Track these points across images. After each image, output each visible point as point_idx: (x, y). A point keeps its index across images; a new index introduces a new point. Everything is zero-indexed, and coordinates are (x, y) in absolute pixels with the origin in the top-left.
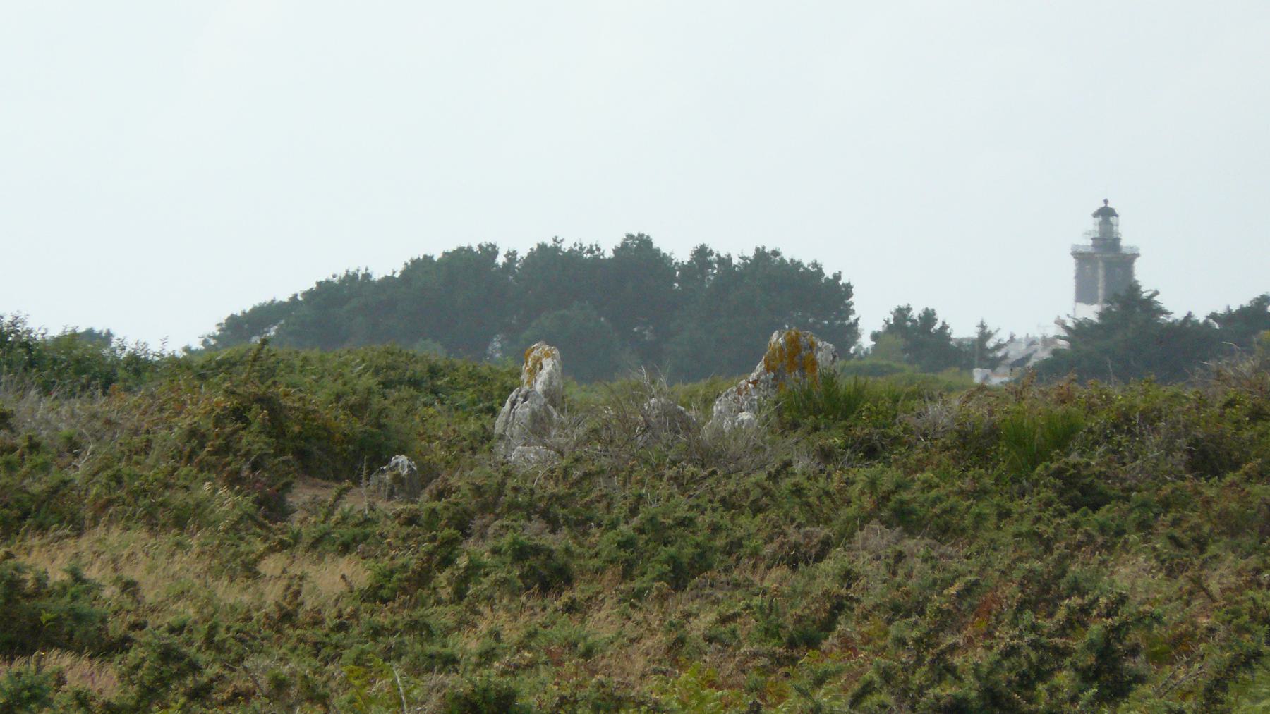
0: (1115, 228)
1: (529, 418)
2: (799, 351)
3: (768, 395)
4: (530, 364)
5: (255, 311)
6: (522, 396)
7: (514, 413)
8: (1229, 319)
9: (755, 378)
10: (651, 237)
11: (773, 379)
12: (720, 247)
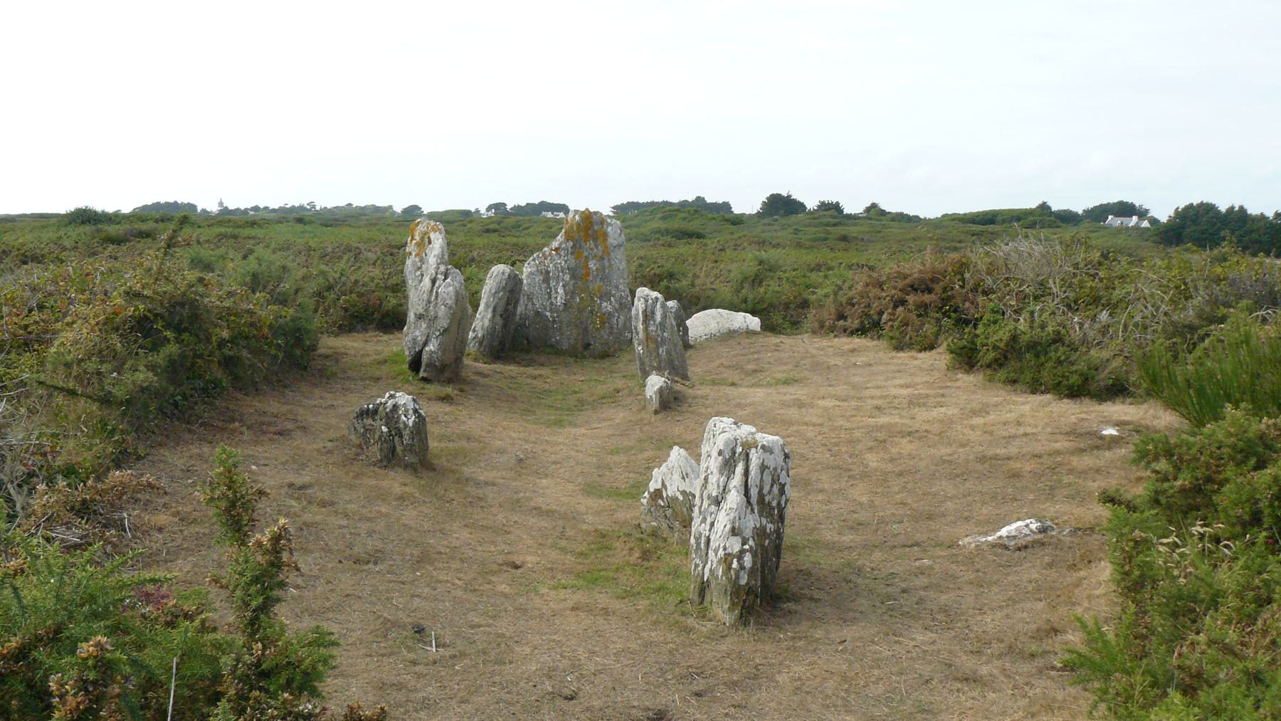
0: (1121, 399)
1: (453, 297)
2: (592, 225)
4: (417, 238)
5: (445, 212)
7: (437, 292)
8: (684, 204)
9: (557, 246)
10: (1245, 207)
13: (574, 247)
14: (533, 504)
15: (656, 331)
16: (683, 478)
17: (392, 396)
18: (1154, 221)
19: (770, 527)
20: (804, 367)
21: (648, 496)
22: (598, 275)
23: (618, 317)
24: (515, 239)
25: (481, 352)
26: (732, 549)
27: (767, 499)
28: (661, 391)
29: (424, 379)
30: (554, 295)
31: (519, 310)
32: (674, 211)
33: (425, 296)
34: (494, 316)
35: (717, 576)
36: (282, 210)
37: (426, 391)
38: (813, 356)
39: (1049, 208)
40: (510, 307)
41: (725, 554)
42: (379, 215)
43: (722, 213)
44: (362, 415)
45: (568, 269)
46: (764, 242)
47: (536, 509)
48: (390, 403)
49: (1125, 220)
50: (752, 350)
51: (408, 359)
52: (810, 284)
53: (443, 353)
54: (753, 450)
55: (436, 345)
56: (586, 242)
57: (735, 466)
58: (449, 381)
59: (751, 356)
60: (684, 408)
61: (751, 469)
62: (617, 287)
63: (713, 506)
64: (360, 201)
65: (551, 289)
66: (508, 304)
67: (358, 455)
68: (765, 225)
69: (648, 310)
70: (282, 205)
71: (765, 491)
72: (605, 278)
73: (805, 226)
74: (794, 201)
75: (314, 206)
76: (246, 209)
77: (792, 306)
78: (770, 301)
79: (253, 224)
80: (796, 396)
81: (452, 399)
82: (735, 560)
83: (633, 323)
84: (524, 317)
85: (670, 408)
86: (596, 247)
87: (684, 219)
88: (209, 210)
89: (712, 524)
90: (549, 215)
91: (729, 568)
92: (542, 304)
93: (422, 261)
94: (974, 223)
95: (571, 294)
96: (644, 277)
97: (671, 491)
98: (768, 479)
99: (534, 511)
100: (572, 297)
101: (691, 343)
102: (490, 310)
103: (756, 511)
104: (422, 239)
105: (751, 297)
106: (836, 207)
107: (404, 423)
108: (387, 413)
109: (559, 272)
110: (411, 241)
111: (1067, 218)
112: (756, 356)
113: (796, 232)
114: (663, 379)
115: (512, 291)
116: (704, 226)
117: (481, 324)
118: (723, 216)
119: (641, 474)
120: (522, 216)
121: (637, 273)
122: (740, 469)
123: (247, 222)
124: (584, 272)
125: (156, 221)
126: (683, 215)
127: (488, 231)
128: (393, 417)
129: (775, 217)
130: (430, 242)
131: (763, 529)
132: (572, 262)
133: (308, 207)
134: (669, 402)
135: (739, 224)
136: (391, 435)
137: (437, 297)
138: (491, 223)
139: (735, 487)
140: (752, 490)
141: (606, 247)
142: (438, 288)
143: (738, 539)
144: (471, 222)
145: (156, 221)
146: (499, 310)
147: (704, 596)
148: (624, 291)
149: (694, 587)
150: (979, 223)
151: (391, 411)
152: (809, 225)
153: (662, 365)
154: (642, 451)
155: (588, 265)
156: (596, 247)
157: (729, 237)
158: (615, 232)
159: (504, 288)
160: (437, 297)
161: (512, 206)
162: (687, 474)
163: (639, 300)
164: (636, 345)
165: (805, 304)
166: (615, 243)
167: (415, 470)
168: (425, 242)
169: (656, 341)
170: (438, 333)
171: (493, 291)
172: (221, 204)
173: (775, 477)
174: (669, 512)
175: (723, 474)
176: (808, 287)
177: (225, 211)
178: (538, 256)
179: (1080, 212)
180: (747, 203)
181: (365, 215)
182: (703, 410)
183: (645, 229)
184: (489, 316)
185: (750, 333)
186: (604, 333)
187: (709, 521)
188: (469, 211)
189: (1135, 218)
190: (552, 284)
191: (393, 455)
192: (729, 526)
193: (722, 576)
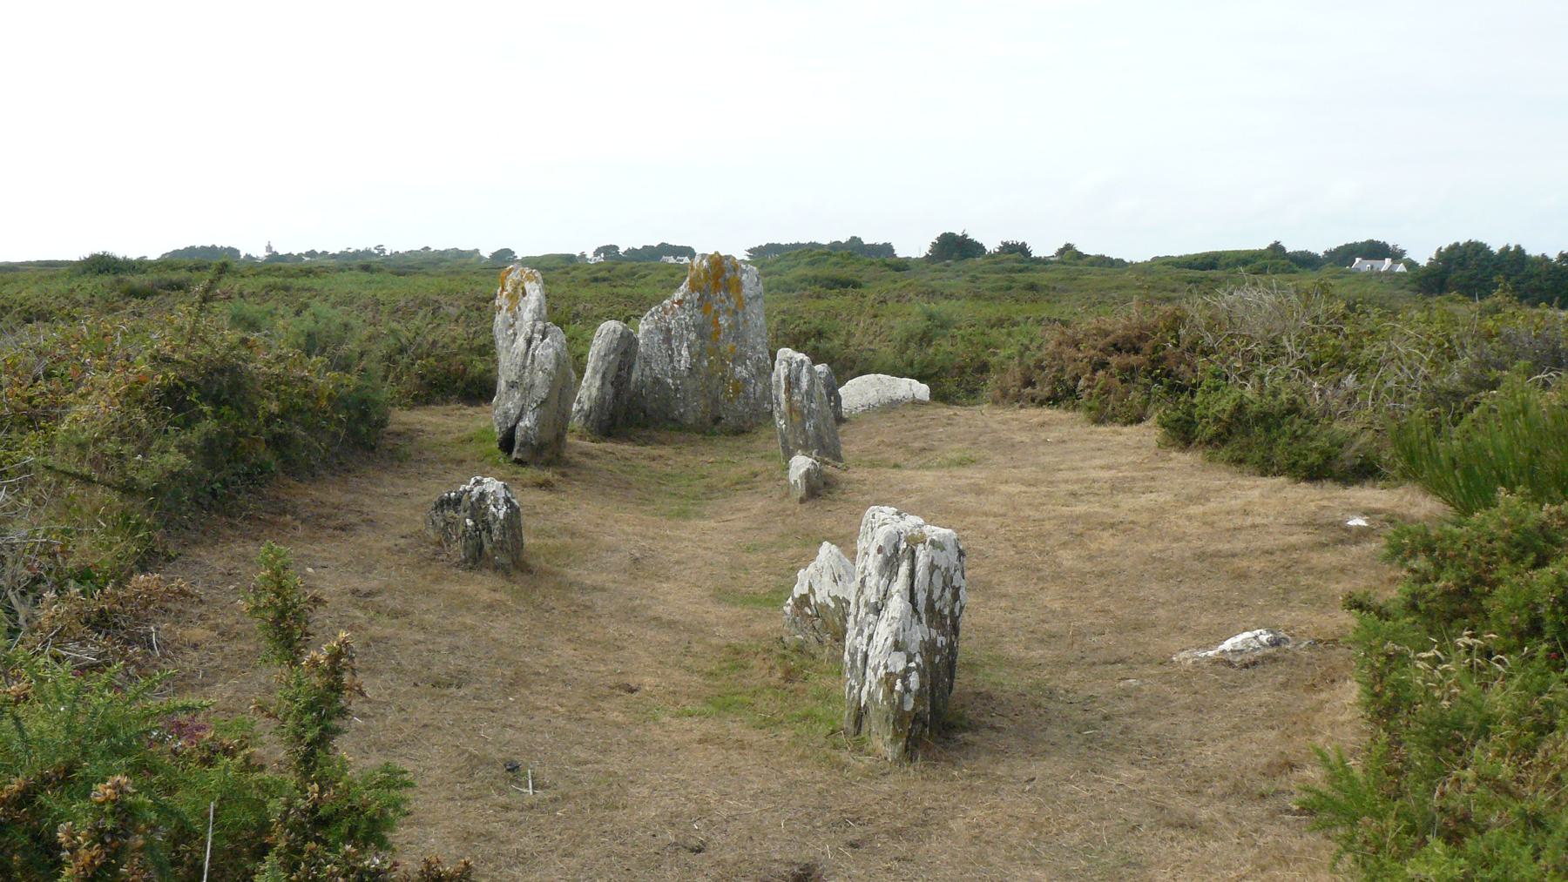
1: (553, 361)
4: (509, 288)
6: (539, 332)
7: (533, 355)
8: (836, 246)
15: (801, 402)
16: (835, 581)
17: (478, 483)
18: (1411, 265)
22: (730, 333)
23: (756, 385)
24: (629, 289)
27: (937, 606)
28: (808, 474)
29: (519, 462)
33: (519, 360)
35: (877, 700)
36: (343, 255)
38: (994, 431)
39: (1283, 249)
41: (886, 673)
42: (462, 261)
45: (694, 325)
48: (476, 490)
49: (1377, 263)
50: (919, 424)
51: (499, 437)
54: (920, 547)
55: (532, 419)
57: (898, 566)
59: (918, 432)
62: (754, 348)
64: (439, 244)
65: (672, 350)
66: (620, 370)
69: (792, 375)
72: (739, 337)
73: (984, 272)
74: (971, 240)
75: (383, 251)
77: (969, 370)
79: (308, 272)
80: (973, 481)
81: (552, 486)
82: (899, 681)
86: (728, 298)
88: (254, 256)
89: (871, 637)
90: (671, 260)
93: (514, 316)
94: (1190, 268)
95: (697, 356)
97: (820, 597)
98: (938, 582)
102: (599, 376)
104: (515, 290)
105: (917, 358)
106: (1022, 249)
108: (472, 503)
109: (682, 329)
111: (1305, 261)
112: (924, 431)
113: (974, 279)
114: (810, 460)
115: (625, 353)
116: (860, 274)
117: (587, 393)
120: (638, 261)
122: (904, 569)
123: (301, 271)
124: (712, 329)
125: (190, 270)
126: (834, 259)
127: (596, 280)
129: (948, 261)
130: (524, 294)
131: (934, 642)
132: (700, 318)
133: (376, 252)
136: (477, 530)
137: (533, 361)
138: (600, 270)
139: (898, 591)
140: (919, 595)
141: (740, 298)
142: (535, 350)
143: (903, 655)
144: (574, 269)
145: (190, 270)
146: (610, 377)
148: (762, 353)
150: (1197, 268)
151: (477, 500)
156: (728, 298)
157: (892, 286)
158: (752, 281)
159: (615, 350)
160: (533, 361)
161: (626, 249)
163: (781, 364)
164: (777, 419)
165: (984, 368)
166: (751, 294)
168: (519, 293)
169: (802, 414)
170: (534, 405)
171: (602, 354)
172: (269, 248)
173: (948, 580)
174: (818, 623)
177: (274, 257)
178: (657, 311)
179: (1321, 254)
180: (913, 245)
184: (598, 383)
185: (916, 403)
186: (739, 406)
187: (866, 633)
189: (1388, 261)
190: (675, 344)
192: (890, 640)
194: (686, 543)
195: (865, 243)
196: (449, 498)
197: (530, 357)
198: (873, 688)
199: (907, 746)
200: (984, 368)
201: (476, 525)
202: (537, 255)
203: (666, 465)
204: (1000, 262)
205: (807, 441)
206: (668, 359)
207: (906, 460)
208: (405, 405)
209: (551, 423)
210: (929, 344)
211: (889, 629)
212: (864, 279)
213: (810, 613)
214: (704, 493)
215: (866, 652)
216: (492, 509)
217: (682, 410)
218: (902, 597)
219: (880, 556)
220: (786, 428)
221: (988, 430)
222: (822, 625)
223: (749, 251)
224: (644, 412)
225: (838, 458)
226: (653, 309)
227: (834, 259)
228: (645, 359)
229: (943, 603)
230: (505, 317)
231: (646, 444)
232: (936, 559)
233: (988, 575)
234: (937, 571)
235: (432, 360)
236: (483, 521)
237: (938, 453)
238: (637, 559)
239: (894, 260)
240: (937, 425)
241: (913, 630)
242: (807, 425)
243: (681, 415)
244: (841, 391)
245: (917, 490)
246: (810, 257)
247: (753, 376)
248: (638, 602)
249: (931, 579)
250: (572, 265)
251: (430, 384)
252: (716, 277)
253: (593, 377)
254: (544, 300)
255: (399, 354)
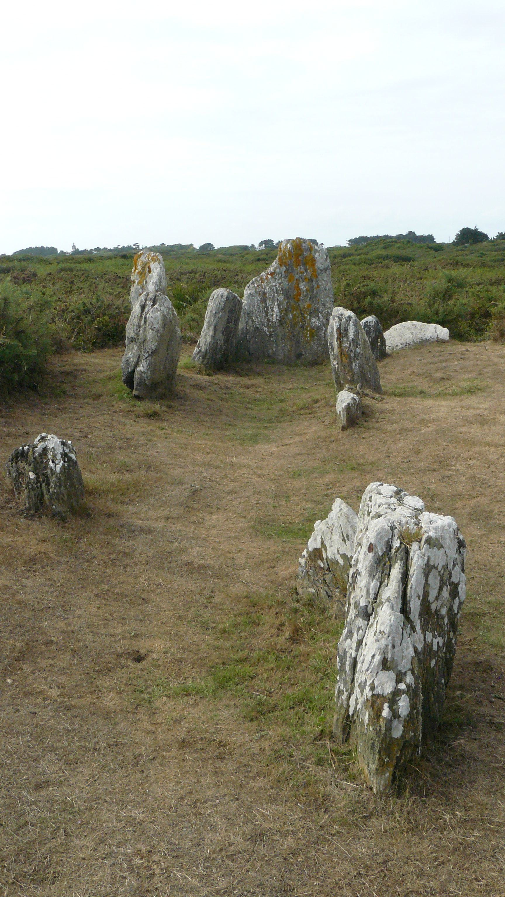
1: (160, 322)
2: (302, 252)
3: (282, 282)
4: (139, 267)
7: (146, 317)
8: (400, 237)
11: (285, 272)
12: (415, 233)
13: (287, 270)
14: (185, 558)
15: (349, 348)
16: (344, 540)
17: (43, 439)
19: (437, 642)
20: (487, 375)
21: (306, 555)
22: (308, 294)
25: (204, 365)
26: (383, 689)
27: (433, 607)
28: (348, 408)
29: (137, 397)
30: (270, 313)
31: (240, 326)
32: (392, 242)
34: (215, 333)
35: (363, 722)
36: (115, 249)
37: (135, 409)
38: (495, 364)
40: (231, 325)
41: (373, 696)
42: (183, 251)
43: (427, 243)
44: (17, 457)
45: (282, 290)
46: (457, 263)
47: (187, 564)
48: (41, 445)
50: (440, 358)
51: (123, 378)
52: (492, 297)
53: (154, 371)
54: (415, 546)
55: (146, 366)
56: (297, 266)
57: (390, 567)
58: (162, 397)
59: (440, 365)
60: (371, 425)
61: (411, 573)
62: (324, 305)
63: (361, 620)
66: (228, 322)
67: (7, 502)
68: (458, 250)
69: (342, 328)
70: (116, 247)
71: (431, 597)
73: (488, 251)
74: (480, 232)
75: (138, 246)
76: (91, 250)
77: (477, 316)
78: (458, 312)
80: (478, 411)
81: (159, 416)
82: (386, 705)
83: (329, 340)
84: (245, 332)
85: (357, 424)
86: (306, 270)
87: (399, 248)
88: (65, 251)
89: (360, 643)
91: (378, 715)
92: (261, 321)
95: (284, 311)
96: (351, 294)
97: (331, 553)
98: (434, 581)
99: (184, 568)
100: (286, 315)
101: (388, 351)
102: (212, 328)
103: (418, 628)
104: (143, 268)
105: (441, 310)
107: (52, 470)
108: (35, 458)
109: (274, 292)
110: (135, 271)
112: (444, 364)
113: (482, 255)
114: (352, 395)
115: (231, 311)
116: (414, 253)
117: (204, 340)
118: (428, 245)
119: (317, 502)
121: (345, 291)
122: (396, 571)
123: (85, 259)
124: (295, 292)
126: (398, 245)
128: (42, 462)
129: (466, 245)
130: (150, 271)
131: (428, 647)
132: (286, 284)
133: (134, 247)
134: (357, 418)
135: (439, 250)
136: (38, 482)
137: (145, 322)
139: (388, 600)
140: (412, 603)
141: (314, 270)
142: (146, 314)
143: (392, 674)
144: (247, 254)
145: (20, 261)
146: (220, 328)
147: (349, 733)
149: (338, 720)
151: (40, 455)
152: (491, 251)
153: (356, 377)
154: (324, 473)
155: (298, 287)
156: (306, 270)
157: (432, 259)
158: (322, 258)
159: (223, 309)
160: (145, 322)
161: (277, 242)
162: (348, 536)
163: (334, 319)
164: (332, 360)
165: (487, 315)
166: (322, 267)
167: (64, 520)
168: (146, 270)
169: (350, 357)
170: (147, 355)
171: (214, 312)
172: (74, 247)
173: (446, 577)
174: (328, 577)
175: (374, 577)
176: (490, 300)
177: (77, 252)
178: (256, 280)
181: (173, 251)
182: (389, 427)
183: (372, 255)
184: (211, 333)
185: (439, 342)
187: (355, 638)
188: (247, 247)
190: (269, 303)
191: (41, 503)
192: (378, 658)
193: (368, 724)
194: (245, 471)
195: (417, 235)
196: (23, 451)
197: (143, 320)
198: (359, 706)
199: (394, 774)
200: (487, 315)
201: (38, 477)
202: (226, 246)
203: (257, 392)
204: (497, 245)
205: (353, 377)
206: (264, 314)
207: (430, 387)
208: (87, 349)
209: (162, 367)
210: (450, 298)
211: (376, 645)
212: (417, 256)
213: (322, 565)
214: (277, 417)
215: (355, 658)
216: (51, 464)
217: (274, 349)
218: (392, 608)
219: (371, 555)
220: (338, 367)
221: (491, 363)
222: (332, 581)
223: (349, 241)
224: (249, 351)
225: (377, 389)
226: (254, 279)
227: (398, 245)
228: (248, 314)
229: (440, 602)
230: (137, 288)
231: (247, 375)
232: (432, 558)
233: (489, 504)
234: (434, 570)
235: (106, 317)
236: (43, 474)
237: (453, 382)
238: (196, 491)
239: (434, 244)
240: (453, 359)
241: (404, 644)
242: (354, 364)
243: (274, 353)
244: (384, 334)
245: (434, 421)
246: (384, 244)
247: (324, 325)
248: (177, 544)
249: (426, 581)
250: (246, 252)
251: (105, 334)
252: (298, 255)
253: (208, 328)
254: (164, 276)
255: (84, 314)
